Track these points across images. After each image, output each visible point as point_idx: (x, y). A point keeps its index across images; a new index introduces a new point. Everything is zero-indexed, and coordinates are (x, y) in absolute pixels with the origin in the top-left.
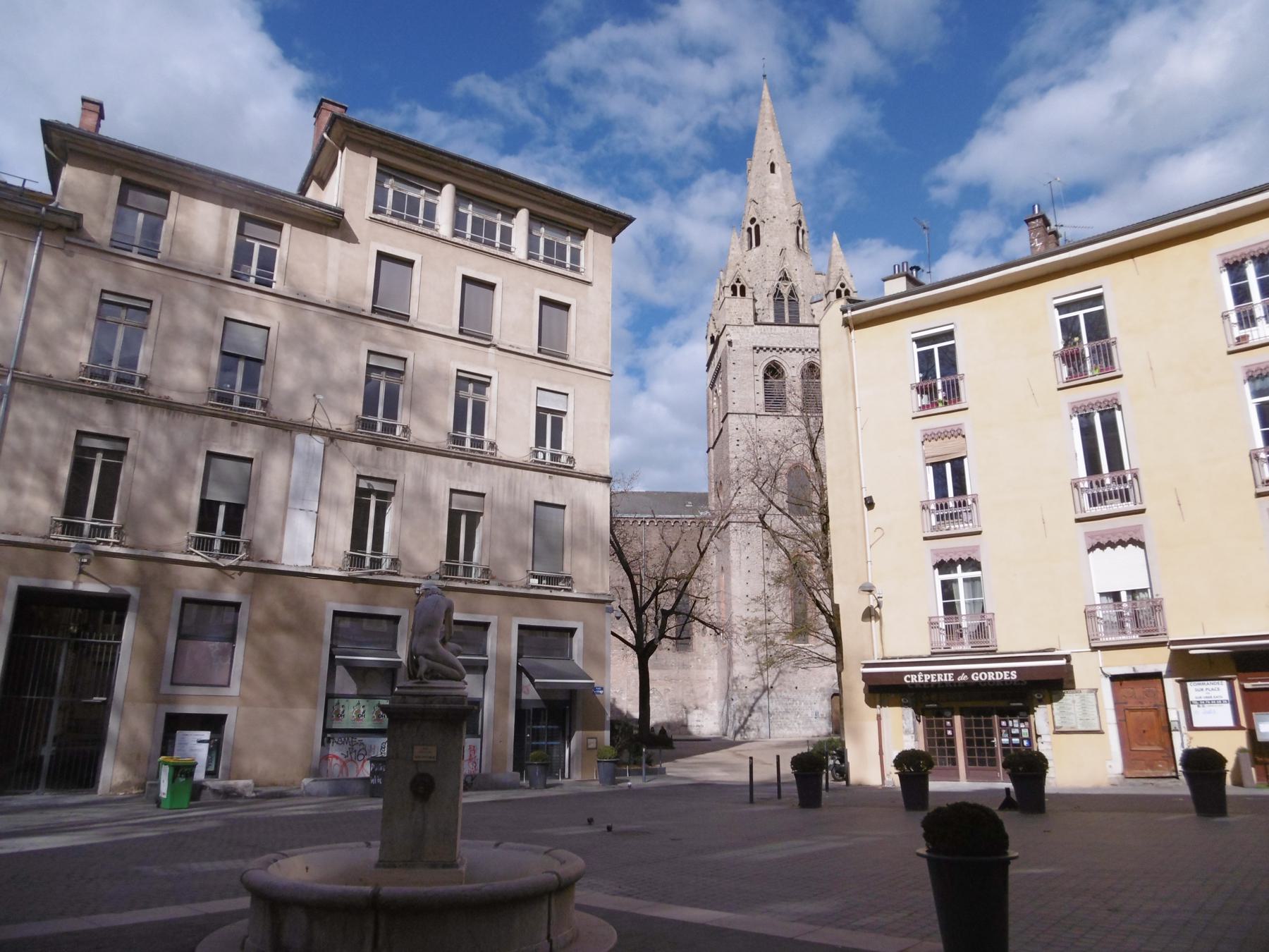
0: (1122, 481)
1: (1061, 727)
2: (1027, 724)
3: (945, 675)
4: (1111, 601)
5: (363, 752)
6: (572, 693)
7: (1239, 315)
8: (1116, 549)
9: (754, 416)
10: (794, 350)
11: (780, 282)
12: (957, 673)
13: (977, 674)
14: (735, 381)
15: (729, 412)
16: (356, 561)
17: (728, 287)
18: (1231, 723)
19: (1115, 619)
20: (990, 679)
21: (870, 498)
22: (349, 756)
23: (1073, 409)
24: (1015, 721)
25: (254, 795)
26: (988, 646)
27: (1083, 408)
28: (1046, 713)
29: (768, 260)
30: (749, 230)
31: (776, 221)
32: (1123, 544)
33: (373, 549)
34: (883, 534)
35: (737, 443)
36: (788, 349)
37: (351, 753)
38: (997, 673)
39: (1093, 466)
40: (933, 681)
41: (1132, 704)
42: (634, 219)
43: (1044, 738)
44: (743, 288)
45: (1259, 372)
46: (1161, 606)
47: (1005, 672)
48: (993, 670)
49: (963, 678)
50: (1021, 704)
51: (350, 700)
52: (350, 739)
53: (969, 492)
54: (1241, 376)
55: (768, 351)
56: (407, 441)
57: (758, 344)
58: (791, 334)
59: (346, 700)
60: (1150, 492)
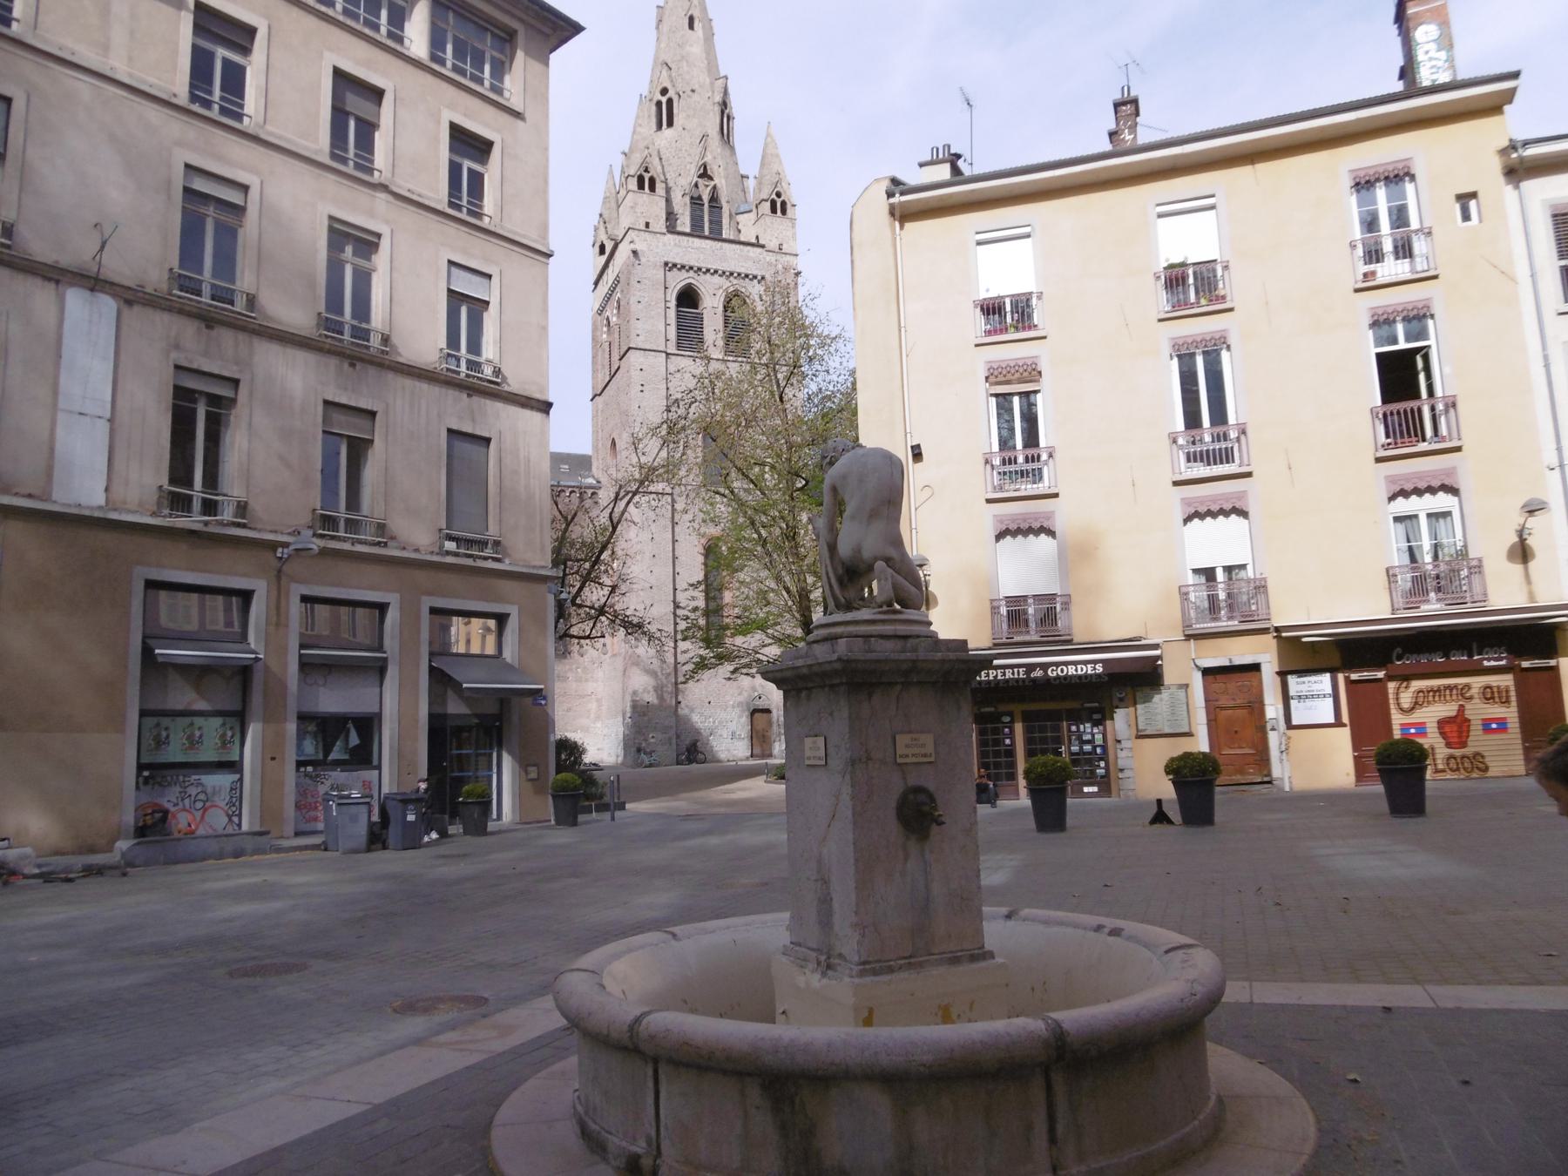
0: (1222, 439)
1: (1145, 730)
2: (1101, 728)
3: (1016, 670)
4: (1203, 579)
5: (202, 797)
6: (504, 699)
7: (1395, 241)
8: (1230, 518)
9: (664, 355)
10: (716, 272)
11: (700, 180)
12: (1030, 668)
13: (1055, 668)
14: (640, 306)
15: (631, 346)
16: (180, 503)
17: (633, 176)
18: (1331, 720)
19: (1206, 604)
20: (1070, 673)
21: (918, 446)
22: (181, 804)
23: (1174, 346)
24: (1088, 725)
25: (37, 871)
26: (1059, 636)
27: (1195, 344)
28: (1128, 714)
29: (684, 149)
30: (659, 104)
31: (695, 97)
32: (1225, 513)
33: (204, 485)
34: (933, 494)
35: (641, 388)
36: (708, 270)
37: (183, 800)
38: (1079, 667)
39: (1192, 420)
40: (999, 678)
41: (1223, 702)
42: (576, 29)
43: (1125, 744)
44: (652, 181)
45: (1385, 316)
46: (1265, 587)
47: (1089, 666)
48: (1075, 663)
49: (1038, 673)
50: (1097, 704)
51: (178, 719)
52: (181, 778)
53: (1042, 443)
54: (1366, 320)
55: (683, 271)
56: (254, 318)
57: (672, 259)
58: (713, 251)
59: (170, 718)
60: (1258, 453)
